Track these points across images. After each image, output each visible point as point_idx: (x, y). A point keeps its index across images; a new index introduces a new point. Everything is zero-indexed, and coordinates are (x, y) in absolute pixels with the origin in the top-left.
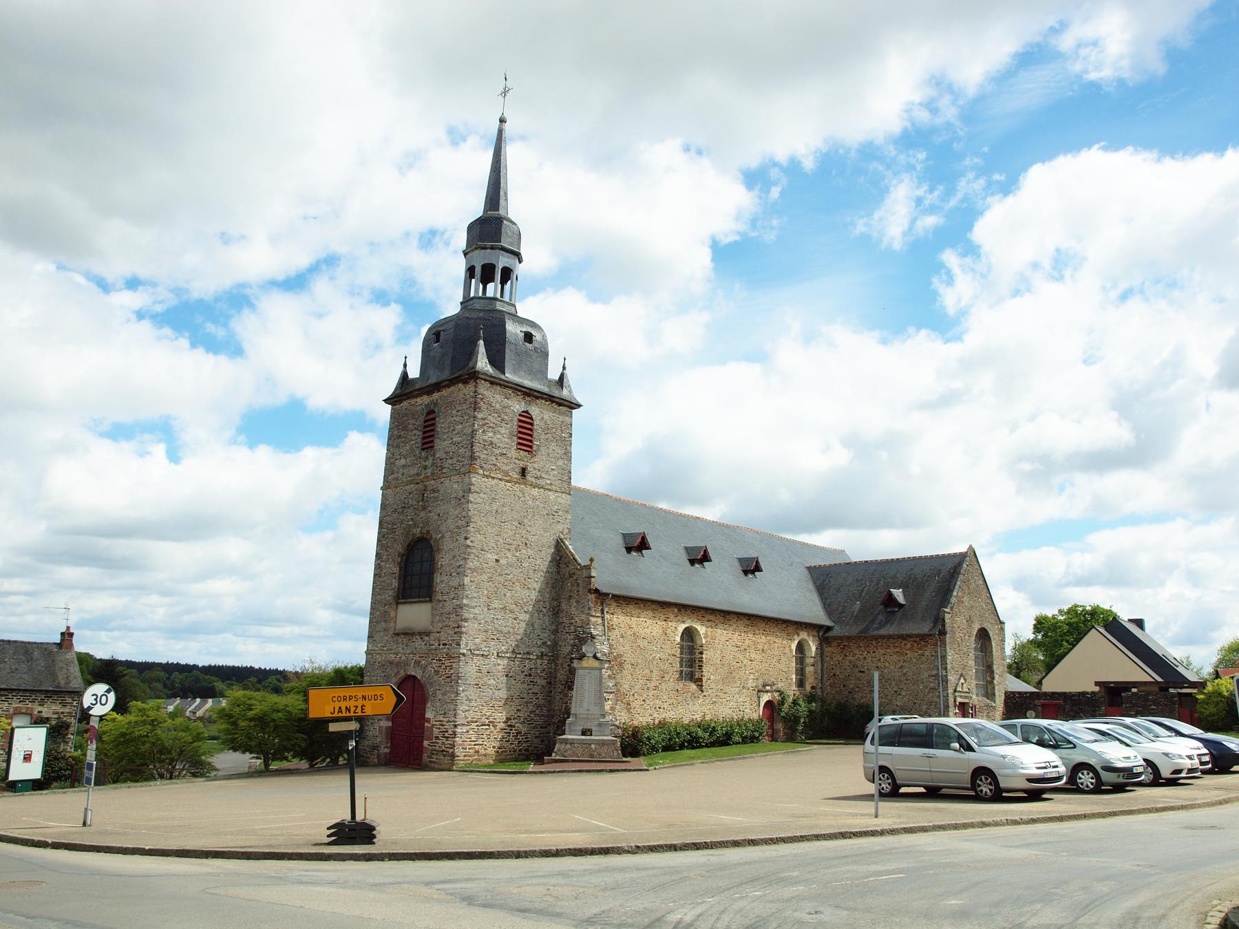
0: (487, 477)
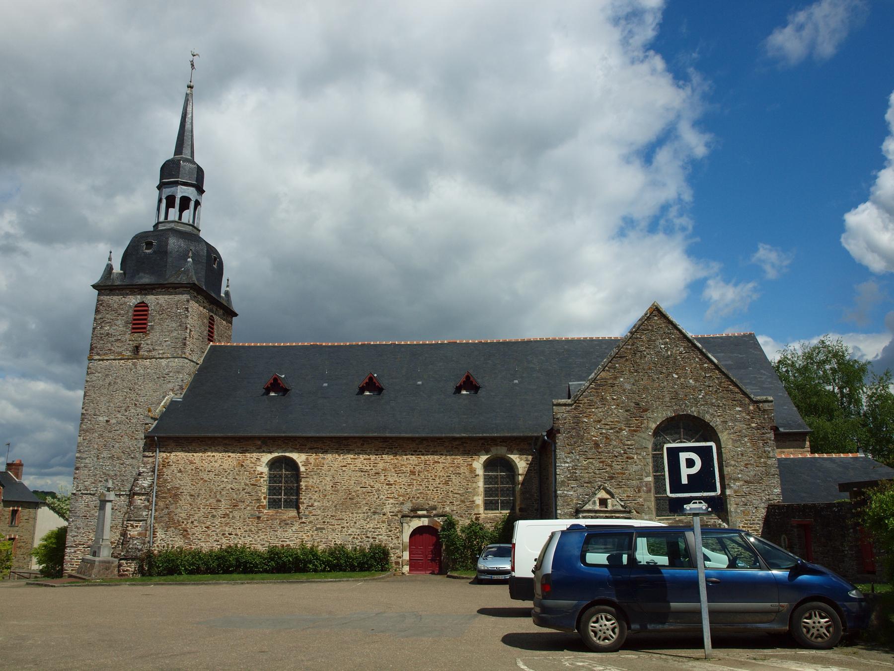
0: (103, 360)
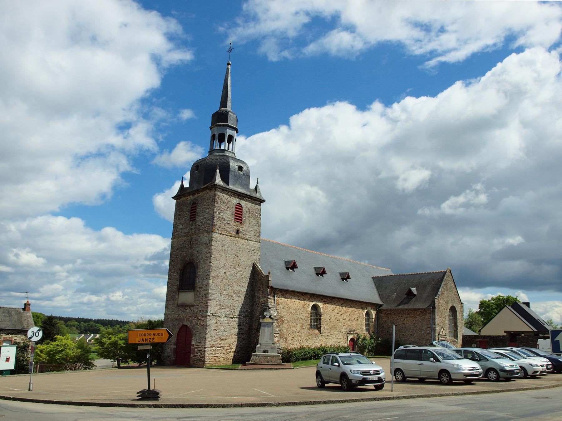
0: (221, 234)
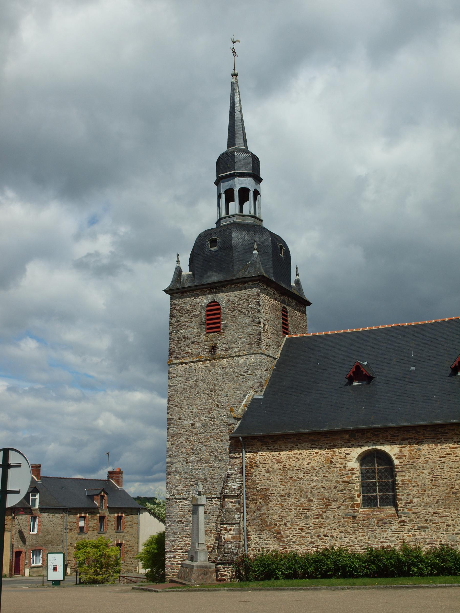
0: (182, 363)
